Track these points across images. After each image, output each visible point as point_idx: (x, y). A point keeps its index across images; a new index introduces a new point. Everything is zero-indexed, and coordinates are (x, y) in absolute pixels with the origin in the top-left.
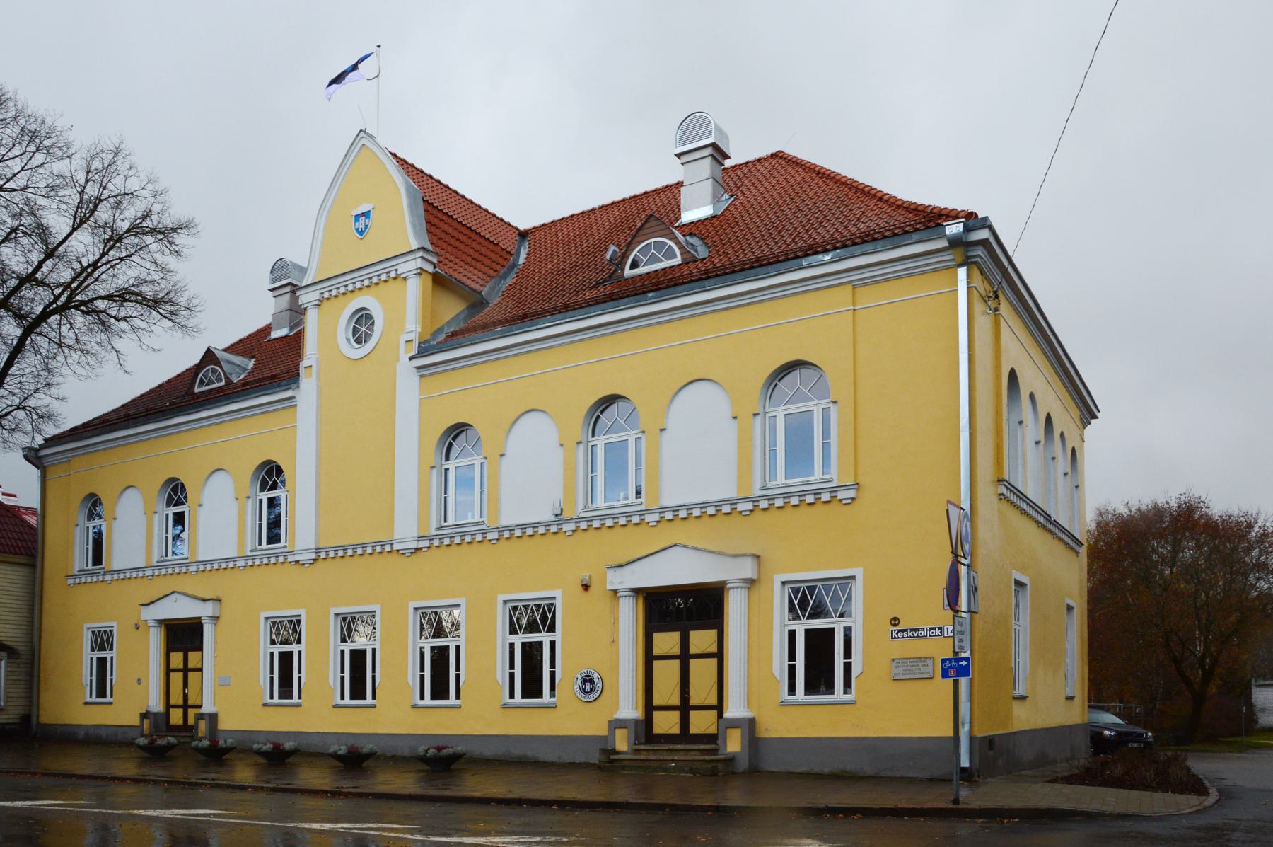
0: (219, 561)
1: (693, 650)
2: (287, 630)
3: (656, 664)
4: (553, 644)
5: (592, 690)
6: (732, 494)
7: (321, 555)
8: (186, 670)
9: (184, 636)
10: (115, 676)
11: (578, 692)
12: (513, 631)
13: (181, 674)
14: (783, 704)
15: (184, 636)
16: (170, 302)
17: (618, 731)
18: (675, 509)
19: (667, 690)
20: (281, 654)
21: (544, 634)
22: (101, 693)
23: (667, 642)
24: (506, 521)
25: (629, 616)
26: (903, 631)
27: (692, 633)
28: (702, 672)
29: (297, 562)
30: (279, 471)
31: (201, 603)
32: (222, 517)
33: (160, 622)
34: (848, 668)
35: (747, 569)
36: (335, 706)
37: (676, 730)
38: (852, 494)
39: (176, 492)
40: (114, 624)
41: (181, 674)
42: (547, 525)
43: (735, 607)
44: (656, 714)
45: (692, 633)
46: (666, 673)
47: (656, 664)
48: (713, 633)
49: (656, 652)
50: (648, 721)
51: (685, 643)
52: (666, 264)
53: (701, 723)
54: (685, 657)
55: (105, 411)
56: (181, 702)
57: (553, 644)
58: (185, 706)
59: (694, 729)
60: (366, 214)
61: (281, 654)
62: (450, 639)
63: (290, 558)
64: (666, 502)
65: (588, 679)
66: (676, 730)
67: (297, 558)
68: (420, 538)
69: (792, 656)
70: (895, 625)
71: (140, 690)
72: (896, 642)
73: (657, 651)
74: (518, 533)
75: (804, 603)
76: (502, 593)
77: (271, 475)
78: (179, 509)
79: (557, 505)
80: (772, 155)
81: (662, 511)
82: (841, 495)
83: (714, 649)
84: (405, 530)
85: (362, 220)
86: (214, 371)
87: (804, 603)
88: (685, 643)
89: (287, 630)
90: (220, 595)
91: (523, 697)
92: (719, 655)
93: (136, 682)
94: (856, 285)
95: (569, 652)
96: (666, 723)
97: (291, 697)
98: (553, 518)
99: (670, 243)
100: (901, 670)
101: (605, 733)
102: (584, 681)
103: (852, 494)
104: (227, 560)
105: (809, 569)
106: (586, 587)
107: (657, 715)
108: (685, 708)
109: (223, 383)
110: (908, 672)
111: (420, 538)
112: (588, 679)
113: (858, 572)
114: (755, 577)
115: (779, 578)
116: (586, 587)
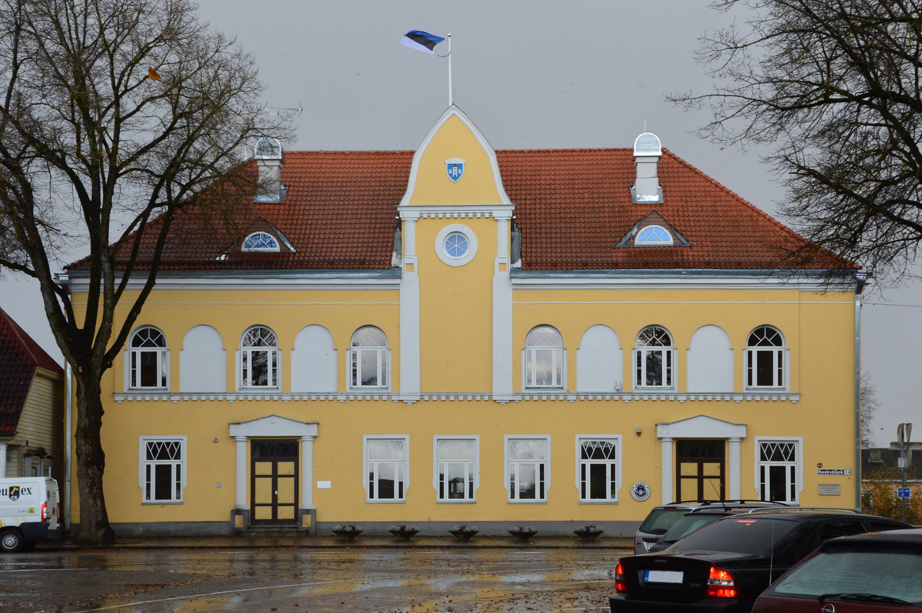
3: (683, 480)
4: (613, 466)
6: (222, 389)
11: (634, 495)
12: (584, 456)
14: (438, 503)
16: (263, 188)
17: (237, 517)
18: (697, 394)
20: (158, 467)
21: (607, 460)
23: (264, 467)
24: (580, 389)
25: (669, 452)
27: (705, 464)
34: (613, 485)
35: (742, 432)
37: (270, 517)
38: (797, 398)
42: (612, 394)
43: (733, 453)
45: (705, 464)
47: (683, 480)
48: (292, 464)
49: (257, 473)
50: (253, 511)
52: (269, 249)
53: (286, 513)
57: (613, 466)
59: (280, 517)
60: (459, 166)
61: (158, 467)
64: (690, 390)
66: (270, 517)
68: (516, 394)
69: (584, 478)
71: (218, 487)
74: (591, 398)
75: (769, 452)
79: (618, 384)
81: (578, 395)
82: (284, 398)
83: (718, 474)
84: (502, 388)
85: (455, 169)
87: (769, 452)
90: (319, 421)
91: (157, 498)
92: (296, 476)
94: (801, 291)
95: (624, 471)
96: (263, 513)
98: (615, 391)
99: (272, 237)
100: (824, 490)
101: (228, 519)
102: (639, 489)
103: (797, 398)
106: (639, 434)
108: (275, 504)
112: (641, 488)
113: (800, 439)
114: (744, 436)
115: (757, 438)
116: (639, 434)
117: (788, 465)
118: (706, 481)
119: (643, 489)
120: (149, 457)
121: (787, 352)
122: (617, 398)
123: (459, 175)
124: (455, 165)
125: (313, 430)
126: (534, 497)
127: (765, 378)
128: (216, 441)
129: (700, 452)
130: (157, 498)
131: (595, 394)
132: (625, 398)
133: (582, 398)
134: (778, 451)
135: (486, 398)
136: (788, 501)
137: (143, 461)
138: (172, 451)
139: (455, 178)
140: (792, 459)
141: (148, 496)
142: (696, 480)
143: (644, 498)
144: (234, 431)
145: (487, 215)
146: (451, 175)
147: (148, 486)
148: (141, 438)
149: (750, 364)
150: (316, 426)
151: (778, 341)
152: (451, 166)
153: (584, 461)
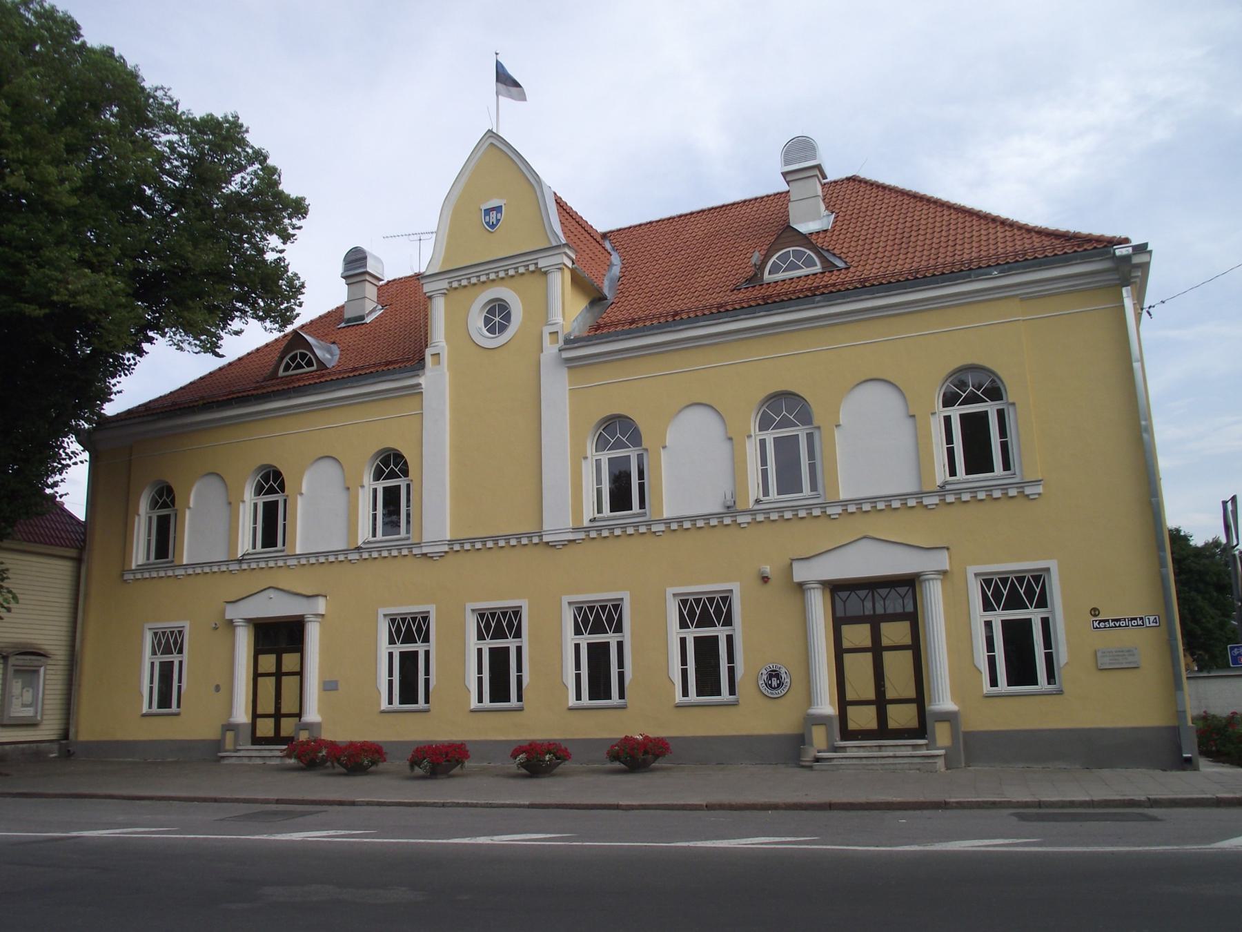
0: (326, 554)
1: (885, 642)
2: (501, 624)
3: (847, 657)
5: (779, 685)
6: (911, 487)
7: (457, 546)
8: (279, 674)
9: (279, 637)
10: (187, 682)
11: (764, 688)
13: (273, 679)
15: (279, 637)
18: (858, 502)
19: (861, 683)
20: (697, 640)
21: (719, 628)
22: (165, 701)
23: (857, 635)
26: (1104, 621)
28: (898, 667)
29: (425, 555)
30: (277, 475)
31: (304, 600)
32: (329, 507)
33: (249, 621)
34: (1049, 659)
36: (678, 706)
39: (272, 481)
40: (670, 591)
41: (273, 679)
43: (935, 598)
44: (850, 709)
46: (860, 668)
47: (847, 657)
48: (298, 655)
51: (876, 635)
54: (877, 650)
55: (162, 394)
56: (272, 710)
57: (730, 639)
58: (278, 716)
60: (498, 209)
61: (697, 640)
62: (419, 644)
63: (415, 551)
65: (774, 674)
67: (425, 550)
70: (1095, 615)
72: (1098, 632)
73: (846, 644)
74: (502, 543)
76: (672, 586)
77: (392, 464)
78: (164, 512)
80: (848, 179)
82: (829, 511)
86: (303, 356)
88: (876, 635)
89: (410, 629)
92: (300, 674)
93: (213, 688)
95: (749, 644)
97: (718, 692)
99: (808, 252)
102: (770, 676)
104: (336, 553)
105: (690, 584)
107: (851, 710)
108: (881, 702)
109: (315, 367)
110: (1115, 665)
111: (576, 530)
112: (774, 674)
115: (972, 570)
117: (720, 632)
118: (887, 655)
119: (778, 676)
120: (683, 625)
121: (1011, 409)
122: (727, 521)
123: (498, 221)
124: (493, 209)
125: (941, 561)
126: (416, 702)
127: (978, 460)
128: (216, 629)
129: (878, 608)
130: (159, 707)
131: (873, 500)
132: (740, 519)
133: (674, 526)
134: (705, 610)
135: (536, 540)
136: (174, 708)
137: (570, 638)
138: (1030, 592)
139: (493, 226)
140: (728, 622)
141: (994, 682)
142: (869, 655)
143: (781, 692)
144: (232, 613)
145: (532, 268)
146: (488, 223)
147: (992, 661)
148: (147, 626)
149: (949, 439)
150: (946, 553)
151: (995, 393)
152: (488, 212)
153: (989, 616)
